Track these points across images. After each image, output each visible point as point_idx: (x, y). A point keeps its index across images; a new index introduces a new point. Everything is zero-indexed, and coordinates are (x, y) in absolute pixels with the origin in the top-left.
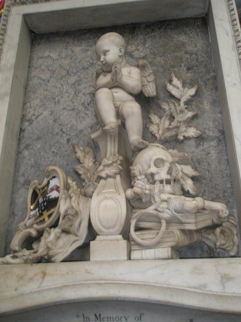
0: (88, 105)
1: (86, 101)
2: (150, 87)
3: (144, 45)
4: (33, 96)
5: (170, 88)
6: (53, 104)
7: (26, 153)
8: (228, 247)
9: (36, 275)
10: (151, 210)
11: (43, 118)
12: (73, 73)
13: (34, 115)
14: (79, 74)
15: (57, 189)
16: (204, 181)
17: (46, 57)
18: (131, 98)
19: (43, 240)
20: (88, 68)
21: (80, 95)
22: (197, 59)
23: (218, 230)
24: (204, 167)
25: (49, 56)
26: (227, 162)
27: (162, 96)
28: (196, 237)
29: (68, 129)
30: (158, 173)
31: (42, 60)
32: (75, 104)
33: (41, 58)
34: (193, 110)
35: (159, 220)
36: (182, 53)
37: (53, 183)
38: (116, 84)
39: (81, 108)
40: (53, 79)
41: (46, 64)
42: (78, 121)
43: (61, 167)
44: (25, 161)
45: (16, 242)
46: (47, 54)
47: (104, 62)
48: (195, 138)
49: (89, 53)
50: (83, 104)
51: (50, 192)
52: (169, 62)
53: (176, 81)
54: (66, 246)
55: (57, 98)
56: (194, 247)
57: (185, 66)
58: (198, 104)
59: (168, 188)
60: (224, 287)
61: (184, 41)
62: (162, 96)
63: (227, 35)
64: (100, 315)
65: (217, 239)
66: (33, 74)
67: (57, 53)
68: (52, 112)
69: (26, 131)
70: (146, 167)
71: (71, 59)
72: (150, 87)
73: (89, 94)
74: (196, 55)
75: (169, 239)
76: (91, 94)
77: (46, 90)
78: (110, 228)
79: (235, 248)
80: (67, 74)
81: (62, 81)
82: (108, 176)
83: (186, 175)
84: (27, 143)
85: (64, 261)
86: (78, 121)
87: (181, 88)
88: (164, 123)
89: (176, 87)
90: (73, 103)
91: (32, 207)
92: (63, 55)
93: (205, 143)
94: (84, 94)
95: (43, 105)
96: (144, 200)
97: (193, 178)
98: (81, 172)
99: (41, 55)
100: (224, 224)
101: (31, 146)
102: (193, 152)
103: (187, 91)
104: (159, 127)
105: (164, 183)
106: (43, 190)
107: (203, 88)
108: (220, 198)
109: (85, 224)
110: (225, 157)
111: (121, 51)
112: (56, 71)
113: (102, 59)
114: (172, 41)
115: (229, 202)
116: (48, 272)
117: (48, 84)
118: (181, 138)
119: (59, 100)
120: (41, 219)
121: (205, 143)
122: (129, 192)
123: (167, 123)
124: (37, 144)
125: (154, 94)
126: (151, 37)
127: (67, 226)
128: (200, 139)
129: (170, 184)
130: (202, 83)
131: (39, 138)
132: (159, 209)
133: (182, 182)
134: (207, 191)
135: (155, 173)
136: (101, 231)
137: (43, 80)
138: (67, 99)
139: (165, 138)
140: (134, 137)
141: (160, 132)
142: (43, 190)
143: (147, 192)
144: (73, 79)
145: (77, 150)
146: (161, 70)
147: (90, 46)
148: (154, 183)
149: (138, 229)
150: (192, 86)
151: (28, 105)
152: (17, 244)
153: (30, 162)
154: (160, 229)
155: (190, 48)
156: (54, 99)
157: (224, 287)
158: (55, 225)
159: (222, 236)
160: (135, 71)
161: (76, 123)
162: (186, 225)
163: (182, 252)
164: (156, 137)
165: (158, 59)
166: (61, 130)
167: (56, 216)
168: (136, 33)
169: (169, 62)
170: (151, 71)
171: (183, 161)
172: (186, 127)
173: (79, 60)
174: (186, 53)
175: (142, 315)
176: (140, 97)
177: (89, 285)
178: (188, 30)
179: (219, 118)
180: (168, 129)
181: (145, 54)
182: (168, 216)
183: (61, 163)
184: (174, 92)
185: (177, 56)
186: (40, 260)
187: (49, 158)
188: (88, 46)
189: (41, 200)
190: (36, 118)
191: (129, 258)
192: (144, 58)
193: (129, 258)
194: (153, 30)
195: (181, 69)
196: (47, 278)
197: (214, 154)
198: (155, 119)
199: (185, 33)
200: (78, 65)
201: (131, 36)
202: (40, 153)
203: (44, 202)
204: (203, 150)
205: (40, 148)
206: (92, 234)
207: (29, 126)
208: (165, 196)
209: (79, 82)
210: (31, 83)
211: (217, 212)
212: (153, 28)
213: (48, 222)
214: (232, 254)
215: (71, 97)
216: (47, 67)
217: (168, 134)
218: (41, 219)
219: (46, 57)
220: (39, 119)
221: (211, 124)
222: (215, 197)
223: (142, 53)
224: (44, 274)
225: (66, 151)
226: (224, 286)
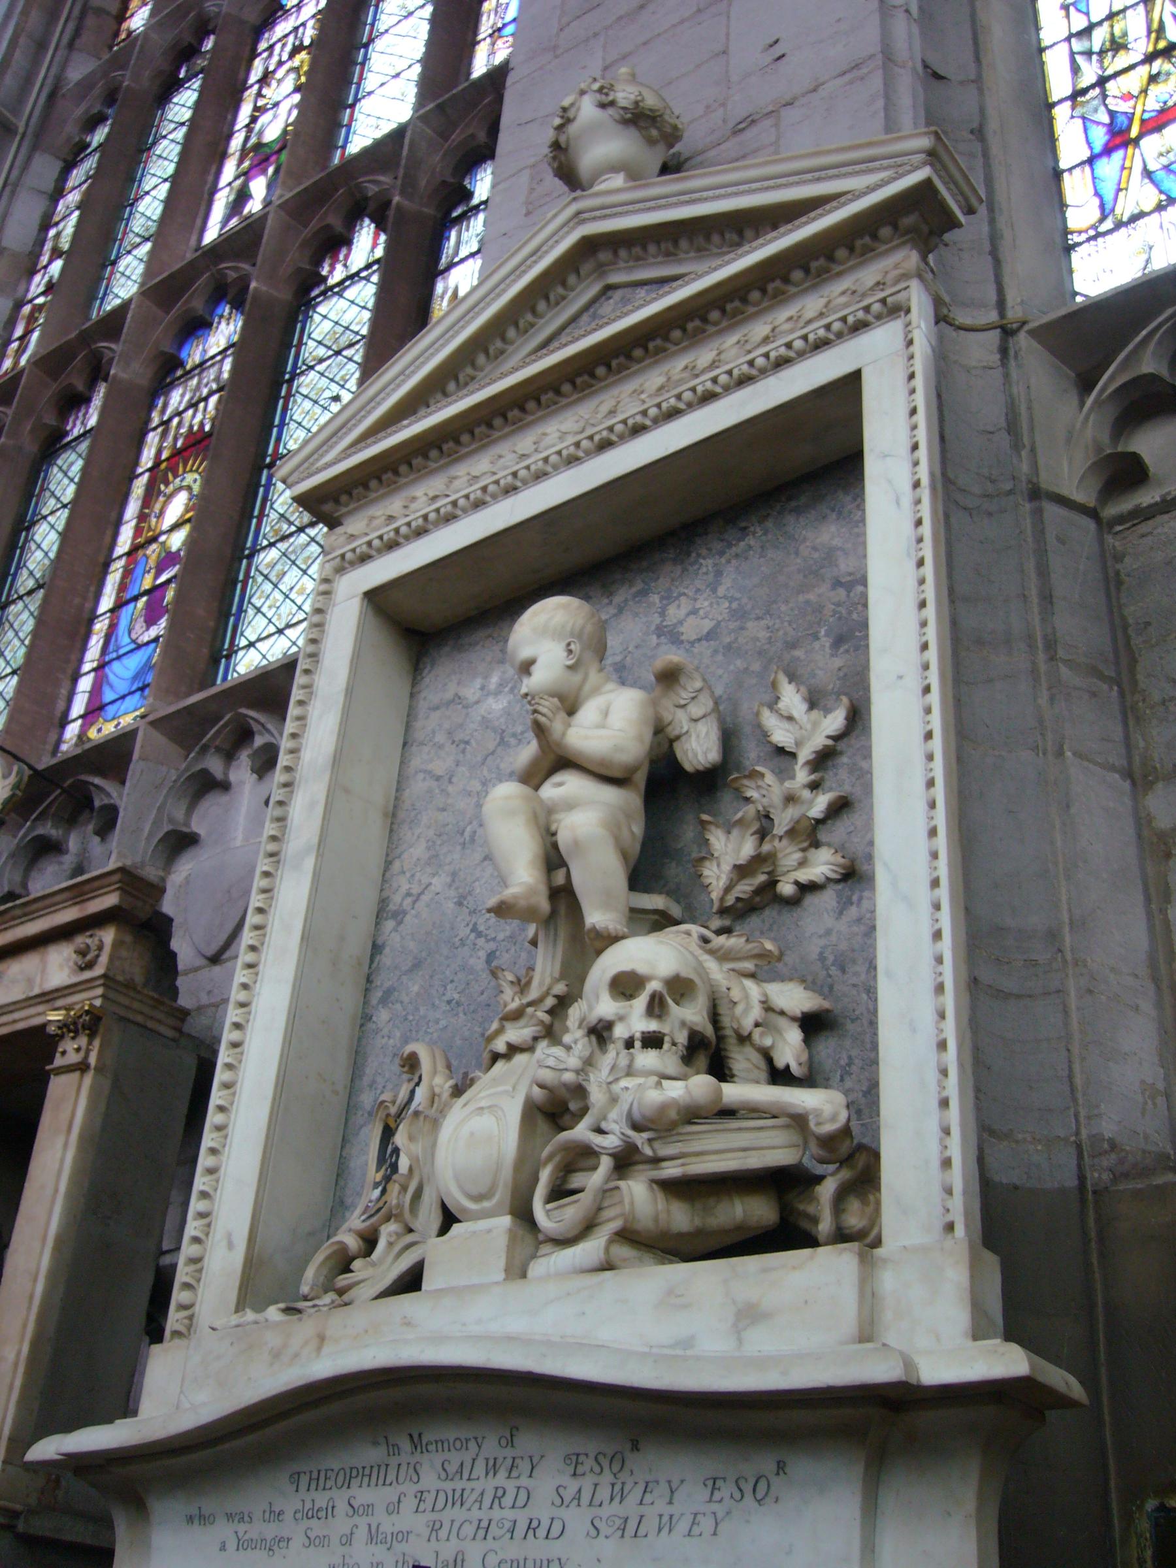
3: (714, 590)
6: (459, 848)
7: (382, 1016)
9: (306, 1343)
11: (432, 899)
13: (409, 894)
24: (854, 980)
30: (621, 1018)
31: (438, 713)
33: (437, 708)
36: (824, 588)
44: (380, 1042)
48: (838, 881)
52: (781, 633)
55: (468, 829)
59: (647, 1059)
60: (740, 1341)
63: (898, 503)
64: (420, 1435)
66: (416, 762)
68: (454, 875)
77: (444, 810)
80: (499, 745)
81: (485, 772)
82: (514, 1049)
84: (387, 984)
85: (376, 1298)
95: (433, 860)
101: (396, 993)
102: (828, 932)
105: (638, 1044)
111: (570, 652)
112: (473, 742)
114: (797, 553)
117: (450, 789)
119: (475, 832)
124: (410, 984)
126: (737, 556)
129: (661, 1048)
131: (417, 965)
132: (604, 1125)
134: (856, 1061)
135: (609, 1017)
136: (464, 1210)
139: (738, 899)
151: (396, 866)
153: (392, 1041)
156: (462, 834)
157: (740, 1341)
162: (664, 1164)
166: (474, 929)
168: (694, 555)
169: (781, 633)
172: (803, 850)
175: (514, 1432)
181: (712, 624)
183: (467, 1034)
185: (807, 602)
187: (437, 1022)
190: (414, 902)
195: (817, 645)
196: (326, 1350)
202: (417, 1009)
205: (418, 994)
207: (395, 930)
210: (407, 793)
212: (743, 524)
217: (745, 888)
220: (421, 904)
223: (707, 621)
224: (322, 1338)
225: (482, 993)
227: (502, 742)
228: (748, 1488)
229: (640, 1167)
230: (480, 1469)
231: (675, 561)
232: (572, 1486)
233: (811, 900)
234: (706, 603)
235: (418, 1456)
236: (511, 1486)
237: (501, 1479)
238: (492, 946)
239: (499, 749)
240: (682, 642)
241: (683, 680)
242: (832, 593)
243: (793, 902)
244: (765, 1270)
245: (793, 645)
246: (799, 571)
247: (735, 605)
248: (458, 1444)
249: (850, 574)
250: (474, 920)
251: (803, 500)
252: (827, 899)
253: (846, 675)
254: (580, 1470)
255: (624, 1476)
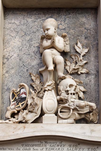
0: (36, 53)
1: (35, 51)
2: (67, 47)
4: (7, 45)
5: (76, 47)
8: (94, 120)
10: (66, 105)
12: (28, 34)
13: (9, 56)
14: (31, 35)
15: (25, 93)
16: (87, 93)
17: (13, 23)
18: (59, 54)
19: (20, 114)
20: (36, 32)
21: (32, 47)
22: (90, 33)
23: (91, 114)
24: (88, 87)
25: (14, 23)
26: (98, 85)
27: (72, 51)
28: (83, 116)
29: (27, 64)
31: (11, 25)
32: (29, 51)
34: (86, 60)
35: (69, 109)
37: (22, 91)
38: (53, 47)
39: (33, 54)
40: (17, 37)
41: (13, 27)
42: (32, 61)
43: (24, 82)
45: (8, 114)
46: (13, 21)
47: (47, 34)
49: (36, 23)
50: (34, 52)
51: (22, 95)
52: (76, 33)
53: (79, 45)
54: (31, 117)
56: (83, 120)
57: (84, 36)
58: (89, 57)
59: (74, 96)
61: (85, 22)
62: (72, 51)
65: (91, 117)
67: (19, 21)
69: (6, 64)
70: (65, 88)
71: (26, 25)
72: (67, 47)
73: (36, 47)
74: (90, 30)
75: (73, 116)
76: (38, 47)
78: (50, 111)
79: (97, 121)
80: (25, 35)
83: (81, 90)
85: (31, 123)
86: (32, 61)
87: (81, 49)
88: (72, 66)
89: (79, 48)
90: (29, 51)
91: (13, 100)
92: (22, 23)
93: (90, 76)
94: (34, 47)
96: (64, 101)
97: (84, 92)
98: (34, 86)
99: (10, 21)
100: (94, 112)
102: (84, 80)
103: (84, 50)
104: (70, 67)
105: (72, 94)
106: (18, 94)
107: (92, 49)
108: (93, 100)
109: (40, 109)
110: (98, 83)
111: (55, 29)
113: (46, 33)
115: (97, 102)
116: (26, 127)
117: (15, 39)
118: (80, 73)
119: (22, 49)
120: (18, 106)
121: (90, 76)
122: (58, 97)
123: (74, 65)
125: (69, 51)
126: (68, 17)
127: (31, 110)
128: (87, 74)
130: (91, 46)
132: (70, 105)
133: (79, 94)
135: (69, 90)
136: (47, 112)
137: (12, 37)
138: (26, 49)
140: (61, 74)
141: (71, 70)
142: (18, 94)
143: (66, 98)
144: (28, 38)
145: (32, 75)
146: (72, 37)
147: (36, 19)
148: (68, 94)
149: (61, 112)
150: (87, 47)
152: (9, 116)
154: (70, 112)
155: (87, 26)
156: (19, 48)
158: (25, 109)
159: (93, 116)
160: (62, 39)
161: (30, 62)
163: (77, 121)
164: (68, 72)
165: (72, 31)
167: (25, 105)
168: (61, 14)
169: (76, 33)
170: (68, 39)
171: (80, 84)
173: (31, 27)
174: (85, 29)
176: (64, 54)
177: (44, 131)
178: (87, 15)
179: (97, 65)
180: (74, 69)
182: (73, 108)
184: (78, 50)
185: (81, 30)
186: (21, 122)
188: (35, 19)
189: (17, 98)
190: (11, 57)
191: (58, 123)
192: (64, 29)
193: (58, 123)
194: (69, 14)
196: (26, 129)
197: (93, 81)
198: (68, 63)
199: (86, 17)
200: (30, 29)
201: (58, 16)
203: (19, 99)
204: (89, 79)
206: (42, 113)
208: (73, 100)
209: (31, 40)
211: (91, 107)
212: (69, 12)
213: (22, 107)
214: (95, 123)
215: (27, 48)
216: (14, 29)
217: (74, 71)
218: (18, 106)
219: (13, 23)
221: (93, 68)
222: (91, 100)
224: (25, 127)
226: (91, 133)
227: (25, 34)
228: (93, 149)
229: (74, 111)
230: (56, 146)
231: (57, 14)
232: (70, 148)
233: (81, 75)
234: (63, 23)
235: (46, 144)
236: (61, 148)
237: (59, 147)
238: (28, 69)
239: (25, 35)
240: (59, 29)
241: (66, 37)
242: (85, 30)
243: (79, 75)
244: (94, 126)
245: (79, 36)
246: (79, 24)
247: (68, 26)
248: (53, 143)
249: (88, 28)
250: (23, 63)
251: (80, 12)
252: (84, 75)
253: (87, 44)
254: (71, 146)
255: (77, 147)
